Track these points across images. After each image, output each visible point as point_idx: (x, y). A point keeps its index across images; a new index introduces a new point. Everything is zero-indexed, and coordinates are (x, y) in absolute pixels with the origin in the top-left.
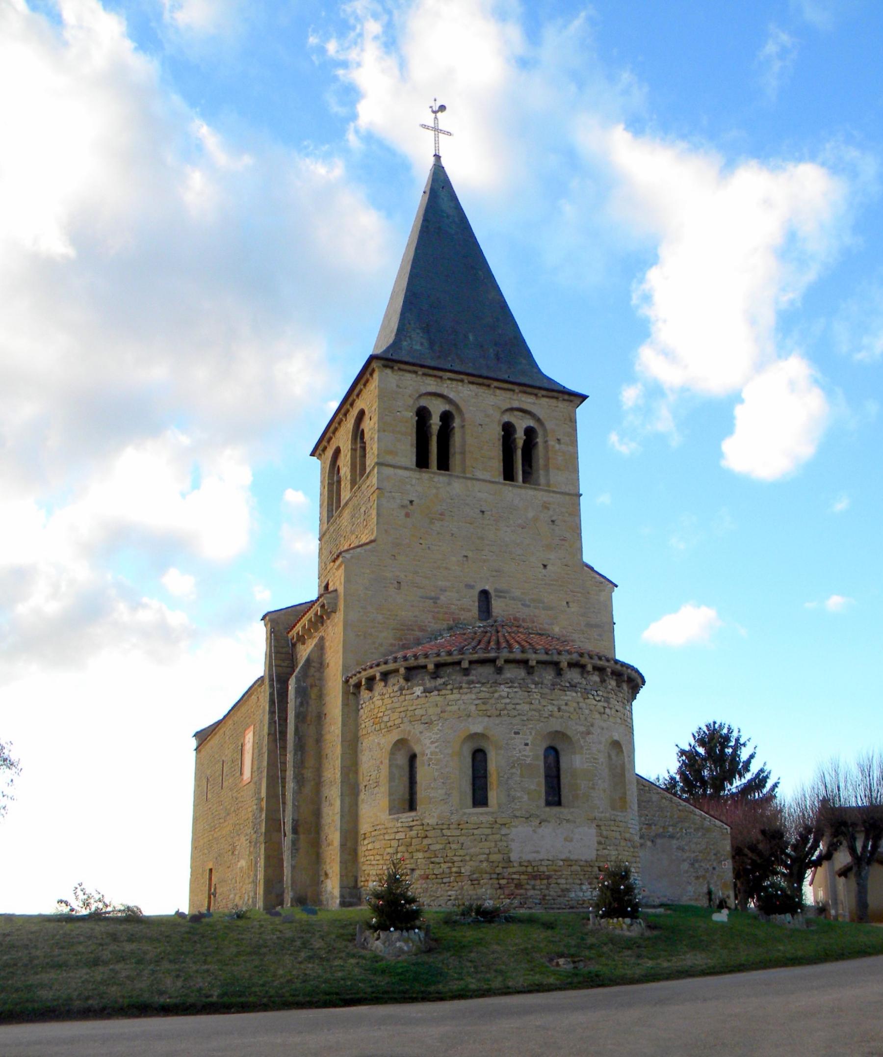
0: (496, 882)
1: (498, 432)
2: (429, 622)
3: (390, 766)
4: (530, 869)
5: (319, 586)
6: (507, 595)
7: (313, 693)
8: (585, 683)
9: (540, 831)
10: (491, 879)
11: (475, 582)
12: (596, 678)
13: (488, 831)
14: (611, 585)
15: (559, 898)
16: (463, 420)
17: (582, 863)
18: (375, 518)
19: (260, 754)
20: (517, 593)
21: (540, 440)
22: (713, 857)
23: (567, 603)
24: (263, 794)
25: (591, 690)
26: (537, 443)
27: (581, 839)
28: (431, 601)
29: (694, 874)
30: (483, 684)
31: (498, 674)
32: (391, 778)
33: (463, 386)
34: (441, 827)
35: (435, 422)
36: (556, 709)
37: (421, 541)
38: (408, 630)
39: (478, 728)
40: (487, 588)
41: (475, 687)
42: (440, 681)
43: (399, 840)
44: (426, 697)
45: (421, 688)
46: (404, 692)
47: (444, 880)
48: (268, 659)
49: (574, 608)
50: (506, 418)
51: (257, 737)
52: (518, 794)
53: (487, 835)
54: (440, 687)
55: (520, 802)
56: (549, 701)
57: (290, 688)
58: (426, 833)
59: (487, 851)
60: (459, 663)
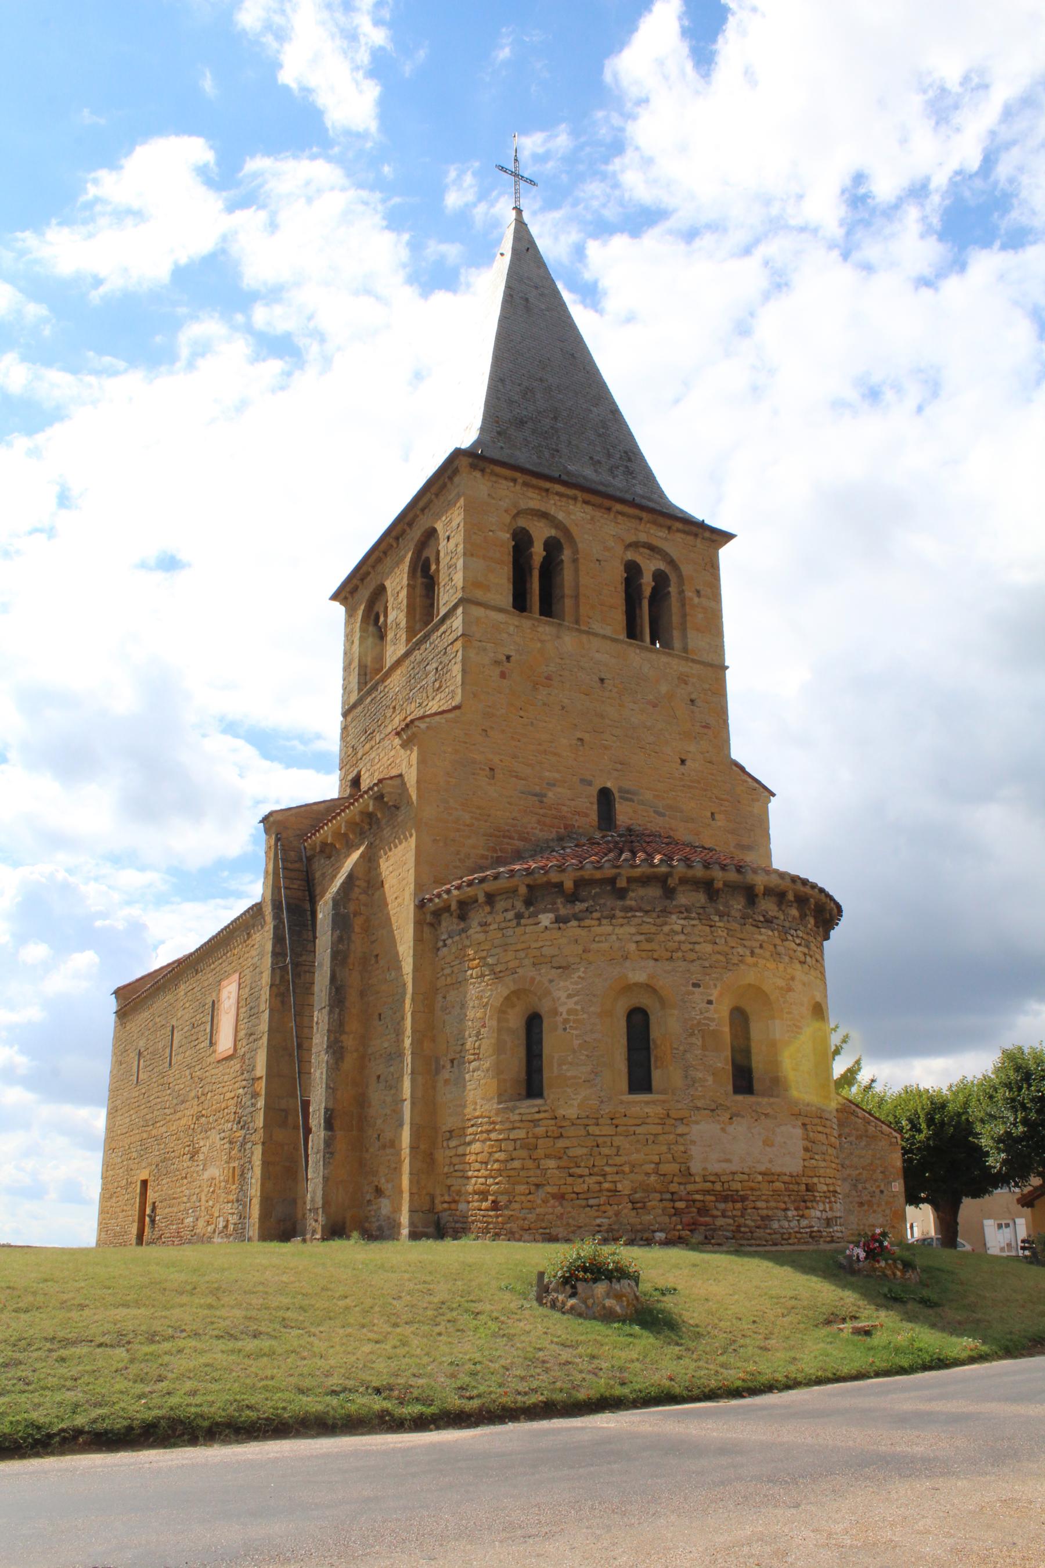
0: (669, 1204)
1: (618, 574)
2: (532, 828)
3: (499, 1030)
4: (718, 1187)
5: (341, 780)
6: (635, 798)
7: (358, 923)
8: (782, 917)
9: (730, 1129)
10: (661, 1200)
11: (594, 776)
12: (794, 912)
13: (658, 1129)
14: (766, 794)
15: (758, 1230)
16: (576, 552)
17: (786, 1178)
18: (459, 677)
19: (253, 1014)
20: (648, 796)
21: (673, 589)
22: (880, 1176)
23: (712, 814)
24: (261, 1070)
25: (790, 929)
26: (669, 593)
27: (785, 1143)
28: (536, 798)
29: (857, 1199)
30: (647, 912)
31: (668, 898)
32: (499, 1048)
33: (575, 505)
34: (585, 1121)
35: (538, 551)
36: (748, 953)
37: (522, 713)
38: (504, 837)
39: (639, 977)
40: (609, 785)
41: (635, 916)
42: (580, 906)
43: (515, 1140)
44: (560, 928)
45: (551, 916)
46: (523, 921)
47: (591, 1202)
48: (271, 877)
49: (721, 821)
50: (630, 555)
51: (247, 990)
52: (700, 1075)
53: (656, 1135)
54: (581, 915)
55: (701, 1086)
56: (739, 941)
57: (320, 916)
58: (560, 1130)
59: (656, 1159)
60: (612, 881)
